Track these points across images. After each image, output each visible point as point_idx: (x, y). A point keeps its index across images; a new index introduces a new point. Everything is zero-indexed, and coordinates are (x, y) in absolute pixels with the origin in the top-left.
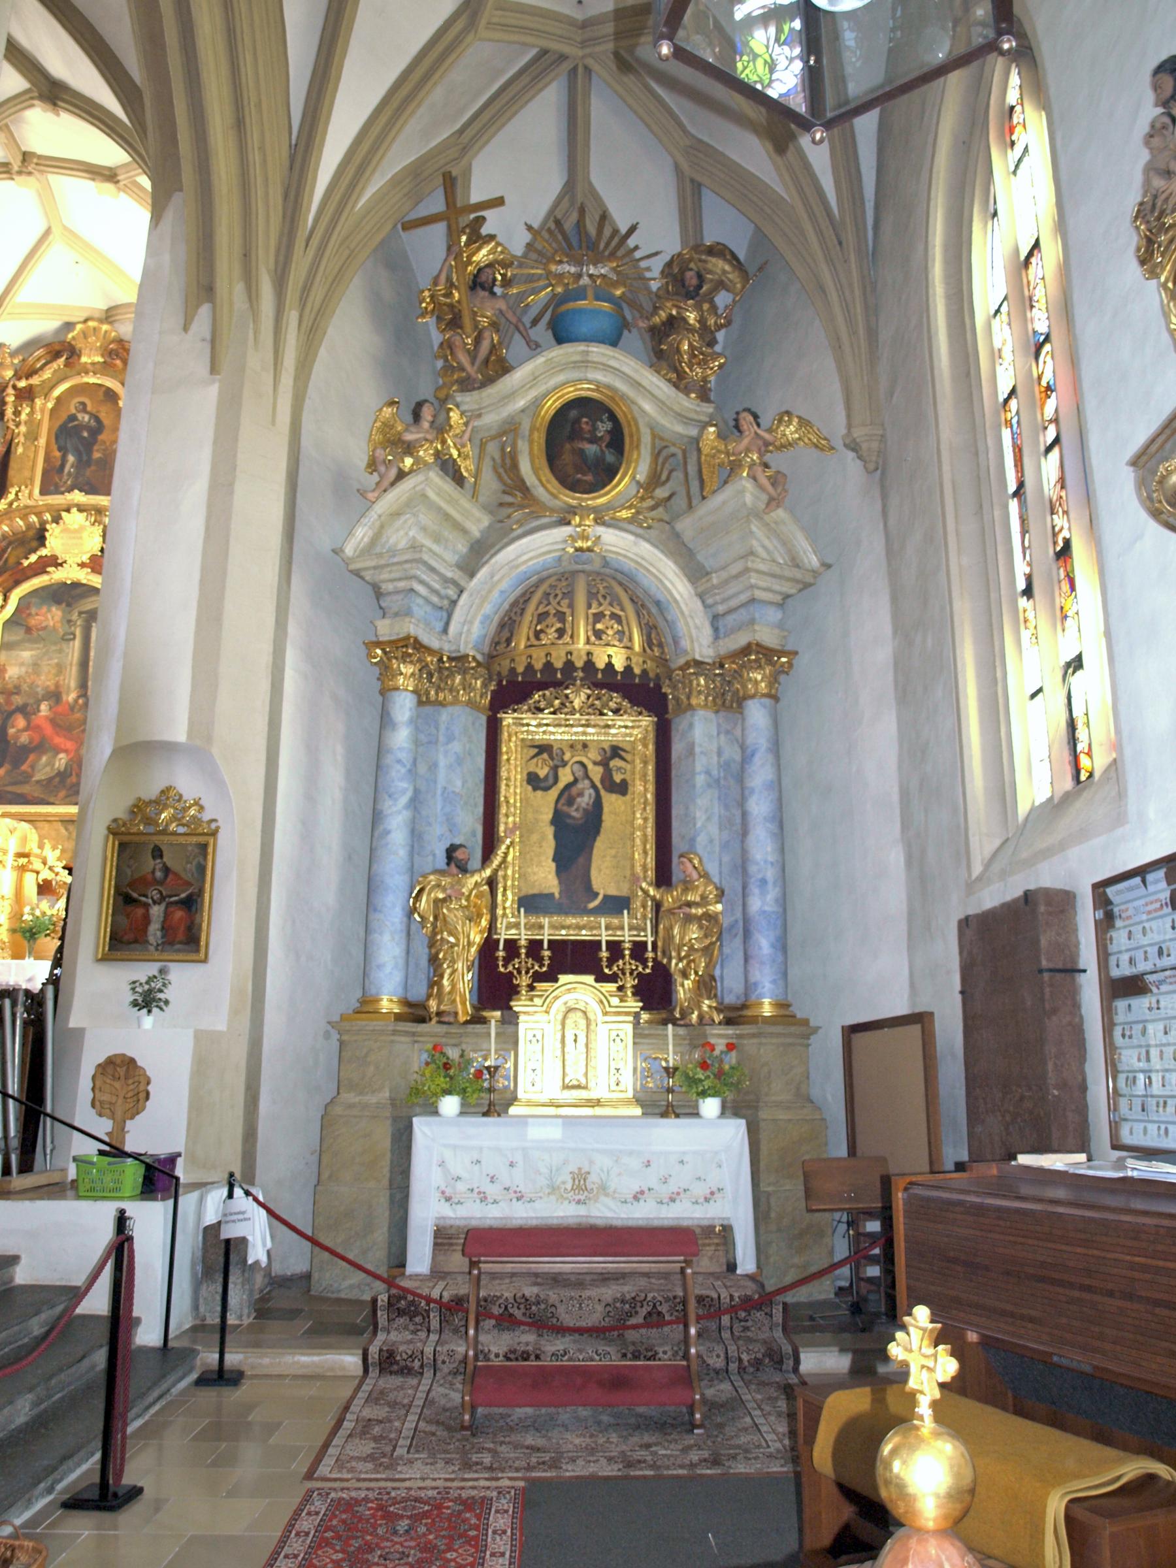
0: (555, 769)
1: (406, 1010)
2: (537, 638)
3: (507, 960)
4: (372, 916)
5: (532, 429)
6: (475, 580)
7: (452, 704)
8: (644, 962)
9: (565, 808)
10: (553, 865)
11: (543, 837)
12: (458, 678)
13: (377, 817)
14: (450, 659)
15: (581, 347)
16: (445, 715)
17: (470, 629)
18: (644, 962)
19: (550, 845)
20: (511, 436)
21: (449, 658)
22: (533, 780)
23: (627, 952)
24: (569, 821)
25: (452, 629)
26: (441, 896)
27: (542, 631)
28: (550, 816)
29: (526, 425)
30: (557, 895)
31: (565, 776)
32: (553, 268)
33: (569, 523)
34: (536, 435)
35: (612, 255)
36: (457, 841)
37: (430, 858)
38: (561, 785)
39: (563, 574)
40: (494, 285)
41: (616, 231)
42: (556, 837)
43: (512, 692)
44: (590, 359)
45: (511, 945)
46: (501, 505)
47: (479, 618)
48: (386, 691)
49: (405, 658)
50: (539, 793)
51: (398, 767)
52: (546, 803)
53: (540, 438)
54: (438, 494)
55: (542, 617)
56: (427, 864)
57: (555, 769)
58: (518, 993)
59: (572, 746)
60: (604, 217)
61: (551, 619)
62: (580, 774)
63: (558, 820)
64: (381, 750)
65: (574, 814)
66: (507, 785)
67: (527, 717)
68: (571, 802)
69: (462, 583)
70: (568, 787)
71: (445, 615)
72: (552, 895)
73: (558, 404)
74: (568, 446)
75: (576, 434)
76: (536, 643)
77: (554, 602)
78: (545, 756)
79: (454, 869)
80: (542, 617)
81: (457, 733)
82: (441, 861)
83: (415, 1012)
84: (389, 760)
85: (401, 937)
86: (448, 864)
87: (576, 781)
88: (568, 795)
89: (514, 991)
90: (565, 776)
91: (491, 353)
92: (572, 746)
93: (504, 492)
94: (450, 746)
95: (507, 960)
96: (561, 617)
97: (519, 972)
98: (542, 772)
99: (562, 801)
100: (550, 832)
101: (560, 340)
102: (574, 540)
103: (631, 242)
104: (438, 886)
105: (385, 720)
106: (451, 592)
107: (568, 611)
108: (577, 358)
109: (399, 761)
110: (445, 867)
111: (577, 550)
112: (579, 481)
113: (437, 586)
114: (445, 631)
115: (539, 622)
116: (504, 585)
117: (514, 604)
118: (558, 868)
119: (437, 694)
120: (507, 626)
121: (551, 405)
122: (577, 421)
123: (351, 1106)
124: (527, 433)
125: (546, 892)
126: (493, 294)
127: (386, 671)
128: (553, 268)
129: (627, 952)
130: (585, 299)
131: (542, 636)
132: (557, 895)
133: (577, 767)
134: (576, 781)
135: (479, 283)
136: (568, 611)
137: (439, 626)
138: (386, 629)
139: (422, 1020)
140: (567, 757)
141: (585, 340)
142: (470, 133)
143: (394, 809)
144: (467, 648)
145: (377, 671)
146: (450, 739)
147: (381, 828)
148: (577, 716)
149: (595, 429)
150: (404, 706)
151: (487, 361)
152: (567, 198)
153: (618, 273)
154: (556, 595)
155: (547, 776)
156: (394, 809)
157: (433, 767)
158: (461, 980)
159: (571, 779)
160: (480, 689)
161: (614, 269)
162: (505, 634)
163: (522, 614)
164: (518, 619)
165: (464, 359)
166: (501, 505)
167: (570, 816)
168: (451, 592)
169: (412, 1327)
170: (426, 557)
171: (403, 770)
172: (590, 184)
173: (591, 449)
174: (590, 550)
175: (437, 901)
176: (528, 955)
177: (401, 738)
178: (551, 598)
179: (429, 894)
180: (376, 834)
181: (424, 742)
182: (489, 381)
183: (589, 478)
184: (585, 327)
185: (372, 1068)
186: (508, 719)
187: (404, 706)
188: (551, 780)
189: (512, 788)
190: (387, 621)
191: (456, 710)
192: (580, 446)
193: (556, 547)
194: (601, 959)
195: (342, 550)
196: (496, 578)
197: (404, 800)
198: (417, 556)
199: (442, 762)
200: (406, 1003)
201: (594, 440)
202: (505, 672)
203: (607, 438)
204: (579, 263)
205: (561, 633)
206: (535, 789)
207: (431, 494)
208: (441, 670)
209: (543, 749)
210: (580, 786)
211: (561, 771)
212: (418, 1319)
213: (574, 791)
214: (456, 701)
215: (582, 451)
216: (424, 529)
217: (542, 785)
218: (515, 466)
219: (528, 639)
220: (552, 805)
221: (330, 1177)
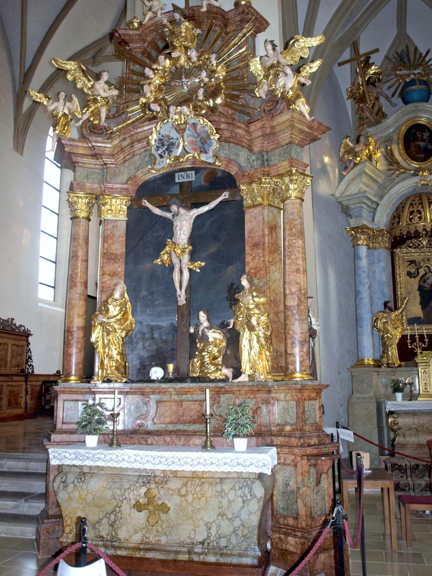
0: (418, 269)
1: (375, 363)
2: (411, 221)
3: (411, 343)
4: (359, 329)
5: (398, 139)
6: (383, 200)
7: (379, 248)
8: (424, 343)
9: (423, 284)
10: (420, 306)
11: (415, 296)
12: (380, 238)
13: (357, 293)
14: (376, 231)
15: (415, 104)
16: (376, 253)
17: (382, 219)
18: (424, 343)
19: (418, 299)
20: (390, 142)
21: (376, 231)
22: (409, 274)
23: (417, 340)
24: (425, 289)
25: (376, 220)
26: (385, 321)
27: (412, 218)
28: (417, 287)
29: (395, 137)
30: (422, 318)
31: (422, 272)
32: (398, 72)
33: (418, 175)
34: (400, 141)
35: (421, 65)
36: (387, 300)
37: (376, 306)
38: (420, 275)
39: (416, 195)
40: (375, 82)
41: (421, 54)
42: (420, 295)
43: (397, 242)
44: (419, 108)
45: (413, 337)
46: (390, 170)
47: (386, 214)
48: (355, 246)
49: (362, 233)
50: (412, 279)
51: (364, 274)
52: (415, 283)
53: (401, 141)
54: (369, 170)
55: (412, 213)
56: (376, 310)
57: (418, 269)
58: (417, 355)
59: (423, 260)
60: (416, 49)
61: (415, 213)
62: (427, 270)
63: (421, 289)
64: (355, 269)
65: (426, 286)
66: (400, 277)
67: (405, 250)
68: (425, 281)
69: (379, 202)
70: (423, 276)
71: (372, 214)
72: (420, 317)
73: (407, 128)
74: (413, 144)
75: (416, 139)
76: (410, 223)
77: (415, 207)
78: (413, 264)
79: (388, 310)
80: (412, 213)
81: (382, 259)
82: (382, 308)
83: (378, 364)
84: (360, 271)
85: (370, 336)
86: (385, 309)
87: (426, 273)
88: (423, 279)
89: (416, 354)
90: (422, 272)
91: (379, 111)
92: (423, 260)
93: (389, 165)
94: (380, 264)
95: (411, 343)
96: (419, 212)
97: (417, 348)
98: (413, 271)
99: (421, 281)
100: (418, 293)
101: (406, 103)
102: (421, 181)
103: (427, 59)
104: (383, 317)
105: (356, 257)
106: (374, 206)
107: (422, 210)
108: (414, 109)
109: (364, 272)
110: (384, 310)
111: (422, 185)
112: (418, 157)
113: (370, 204)
114: (373, 220)
115: (411, 215)
116: (394, 201)
117: (397, 208)
118: (422, 307)
119: (373, 245)
120: (396, 217)
121: (404, 129)
122: (415, 133)
123: (359, 398)
124: (396, 140)
125: (418, 316)
126: (375, 86)
127: (355, 239)
128: (398, 72)
129: (417, 340)
130: (416, 85)
131: (413, 220)
132: (422, 318)
133: (426, 268)
134: (426, 273)
135: (371, 83)
136: (422, 210)
137: (371, 219)
138: (353, 222)
139: (380, 366)
140: (422, 265)
141: (416, 102)
142: (359, 23)
143: (364, 290)
144: (382, 227)
145: (351, 239)
146: (380, 261)
147: (360, 297)
148: (425, 248)
149: (423, 136)
150: (363, 251)
151: (377, 113)
152: (398, 40)
153: (424, 71)
154: (416, 204)
155: (414, 272)
156: (364, 290)
157: (374, 272)
158: (393, 352)
159: (424, 273)
160: (386, 241)
161: (422, 69)
162: (397, 220)
163: (403, 212)
164: (401, 214)
165: (368, 114)
166: (390, 170)
167: (424, 287)
168: (374, 206)
169: (400, 475)
170: (368, 195)
171: (366, 275)
172: (407, 34)
173: (422, 144)
174: (427, 185)
175: (384, 323)
176: (419, 341)
177: (364, 263)
178: (414, 205)
179: (381, 320)
180: (358, 299)
181: (371, 263)
182: (378, 122)
183: (423, 156)
184: (415, 96)
185: (365, 385)
186: (398, 251)
187: (363, 251)
188: (416, 274)
189: (402, 277)
190: (353, 220)
191: (381, 250)
192: (418, 143)
193: (412, 185)
194: (408, 343)
195: (334, 194)
196: (391, 199)
197: (367, 286)
198: (364, 195)
199: (377, 270)
200: (375, 360)
201: (423, 140)
202: (398, 235)
203: (428, 139)
204: (410, 70)
205: (420, 218)
206: (410, 277)
207: (367, 170)
208: (373, 236)
209: (412, 262)
210: (428, 275)
211: (420, 270)
212: (403, 471)
213: (426, 277)
214: (380, 247)
215: (419, 145)
216: (364, 183)
217: (413, 276)
218: (392, 154)
219: (407, 222)
220: (418, 283)
221: (353, 424)
